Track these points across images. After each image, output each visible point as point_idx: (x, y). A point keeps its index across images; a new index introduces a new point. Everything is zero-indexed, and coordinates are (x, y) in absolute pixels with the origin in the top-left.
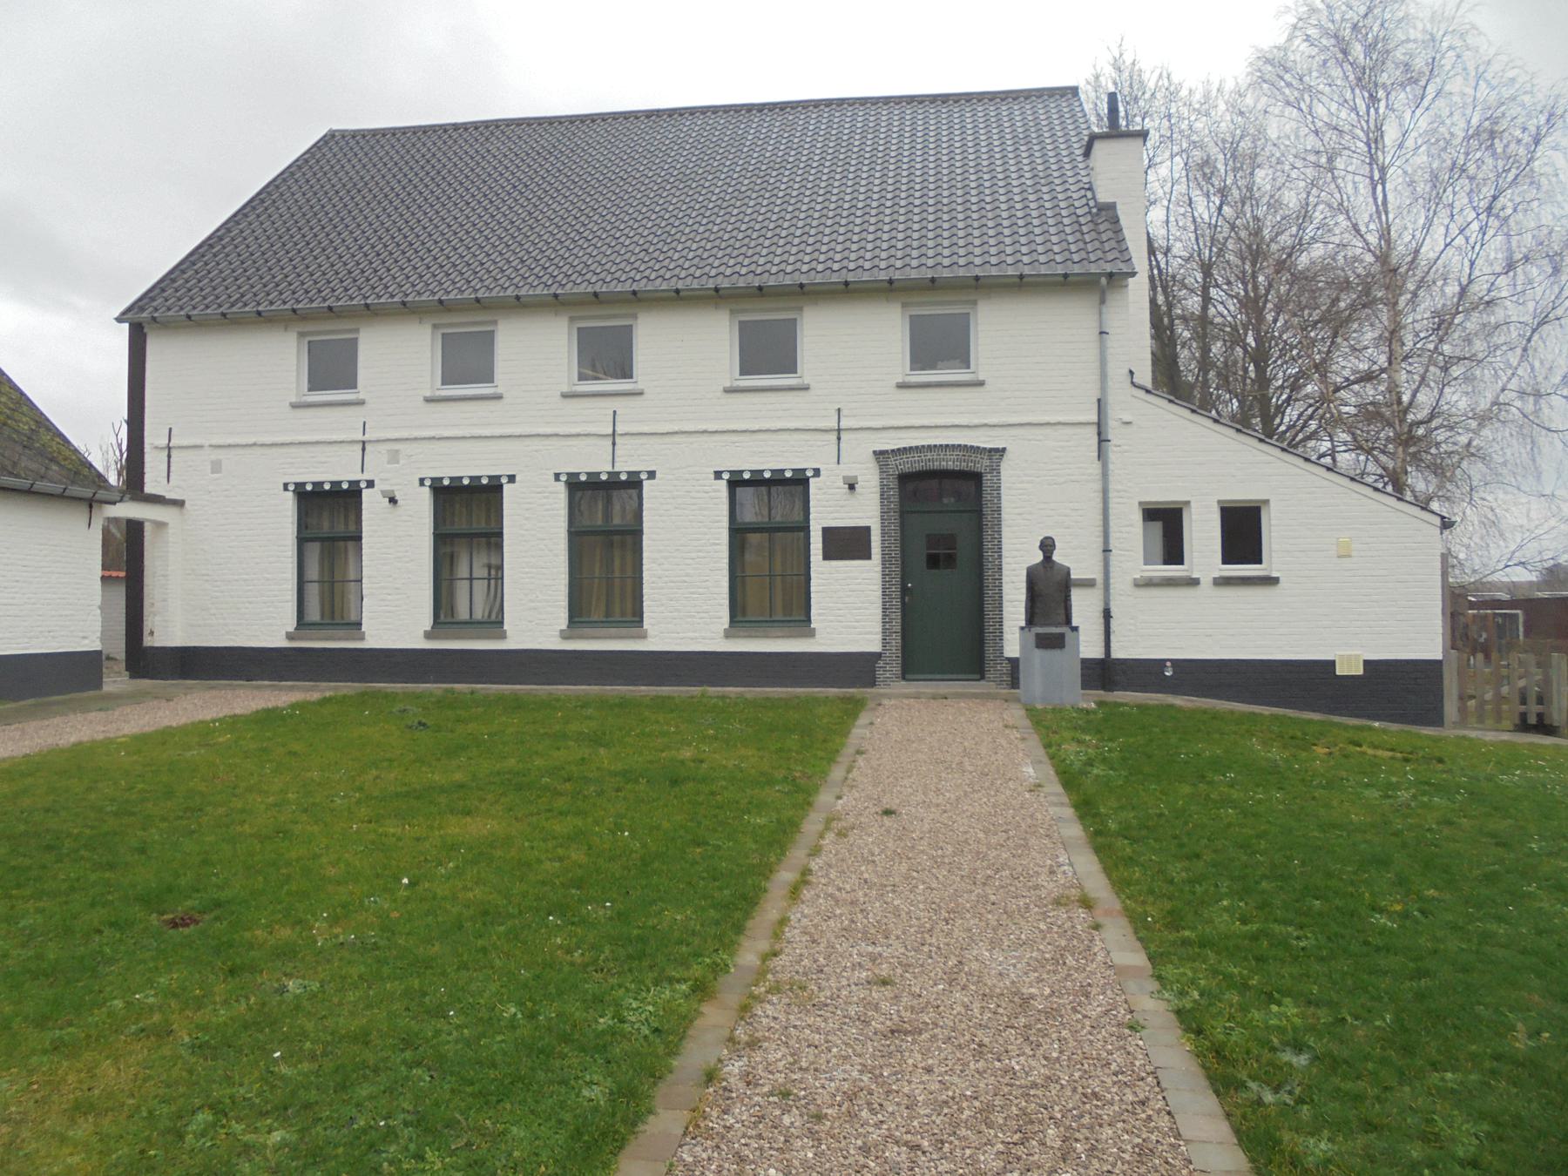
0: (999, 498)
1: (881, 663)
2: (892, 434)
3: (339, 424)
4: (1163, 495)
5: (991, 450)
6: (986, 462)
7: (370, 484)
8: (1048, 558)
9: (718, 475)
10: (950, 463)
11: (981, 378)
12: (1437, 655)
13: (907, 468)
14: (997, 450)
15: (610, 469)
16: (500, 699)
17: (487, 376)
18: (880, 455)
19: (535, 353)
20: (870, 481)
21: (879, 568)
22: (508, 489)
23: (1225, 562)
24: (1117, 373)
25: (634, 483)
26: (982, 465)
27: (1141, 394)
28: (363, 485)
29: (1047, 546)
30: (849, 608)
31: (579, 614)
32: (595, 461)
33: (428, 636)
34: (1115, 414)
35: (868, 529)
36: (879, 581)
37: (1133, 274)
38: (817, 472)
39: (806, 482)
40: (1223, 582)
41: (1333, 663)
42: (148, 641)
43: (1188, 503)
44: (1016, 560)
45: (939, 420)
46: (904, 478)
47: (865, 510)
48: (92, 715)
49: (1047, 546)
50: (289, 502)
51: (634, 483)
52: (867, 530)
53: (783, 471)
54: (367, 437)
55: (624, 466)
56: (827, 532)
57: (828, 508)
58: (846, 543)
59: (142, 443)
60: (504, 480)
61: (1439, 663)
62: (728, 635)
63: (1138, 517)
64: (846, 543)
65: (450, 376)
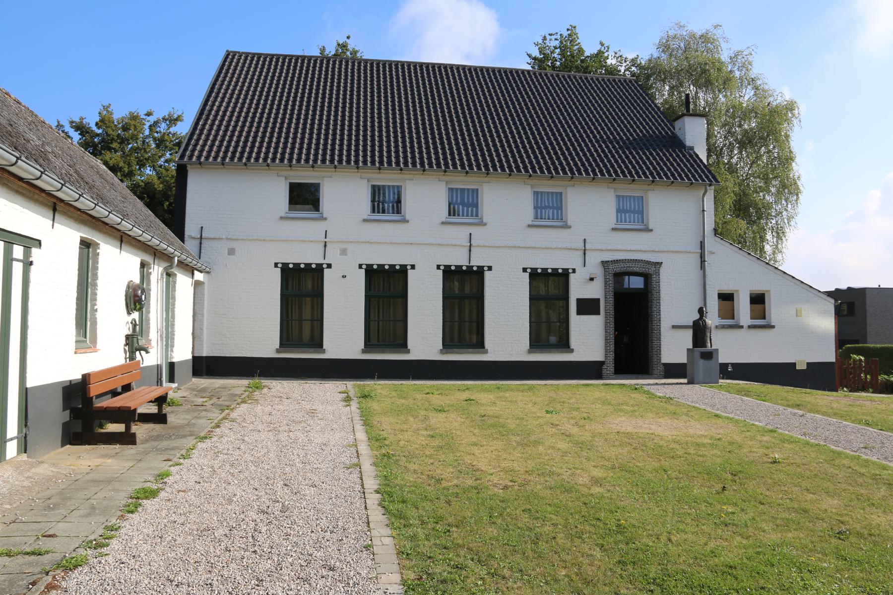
1: (605, 367)
2: (610, 253)
4: (727, 288)
6: (653, 269)
9: (525, 270)
12: (685, 362)
13: (618, 270)
14: (658, 263)
16: (630, 385)
18: (604, 263)
20: (599, 272)
22: (327, 272)
23: (751, 318)
25: (480, 272)
26: (652, 270)
28: (325, 266)
30: (589, 338)
31: (449, 343)
32: (458, 259)
33: (278, 351)
35: (598, 300)
38: (574, 271)
40: (750, 327)
41: (795, 364)
42: (829, 355)
43: (768, 291)
45: (631, 247)
47: (596, 291)
48: (840, 393)
50: (276, 275)
51: (480, 272)
52: (598, 300)
53: (300, 264)
55: (476, 262)
56: (579, 301)
57: (578, 289)
58: (588, 307)
61: (684, 365)
62: (442, 352)
64: (588, 307)
65: (452, 212)
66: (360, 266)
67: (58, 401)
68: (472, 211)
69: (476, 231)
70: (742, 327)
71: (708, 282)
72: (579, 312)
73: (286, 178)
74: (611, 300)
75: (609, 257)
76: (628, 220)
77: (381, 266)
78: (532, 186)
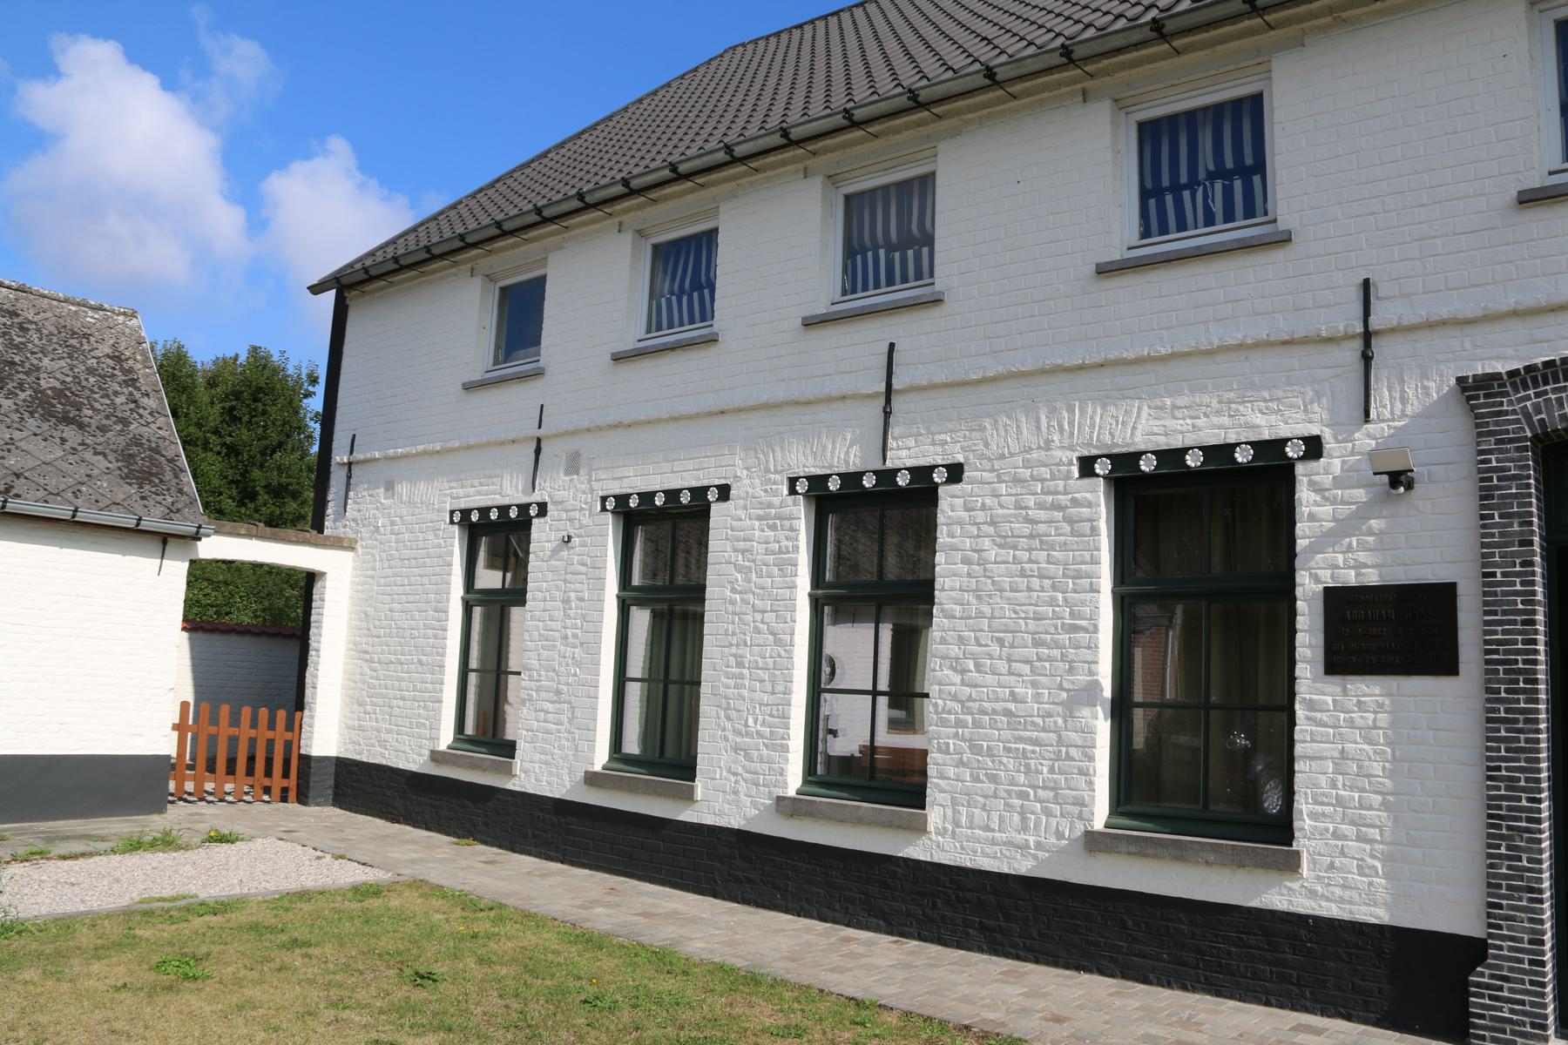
1: (1482, 975)
7: (955, 473)
15: (879, 466)
18: (1477, 391)
19: (1038, 199)
22: (950, 502)
32: (842, 453)
35: (1445, 594)
50: (1097, 504)
53: (1138, 455)
54: (358, 456)
55: (906, 454)
57: (1338, 544)
58: (1394, 631)
64: (1394, 631)
66: (1087, 466)
67: (311, 794)
68: (918, 259)
73: (640, 233)
75: (1501, 355)
76: (1218, 208)
77: (1171, 457)
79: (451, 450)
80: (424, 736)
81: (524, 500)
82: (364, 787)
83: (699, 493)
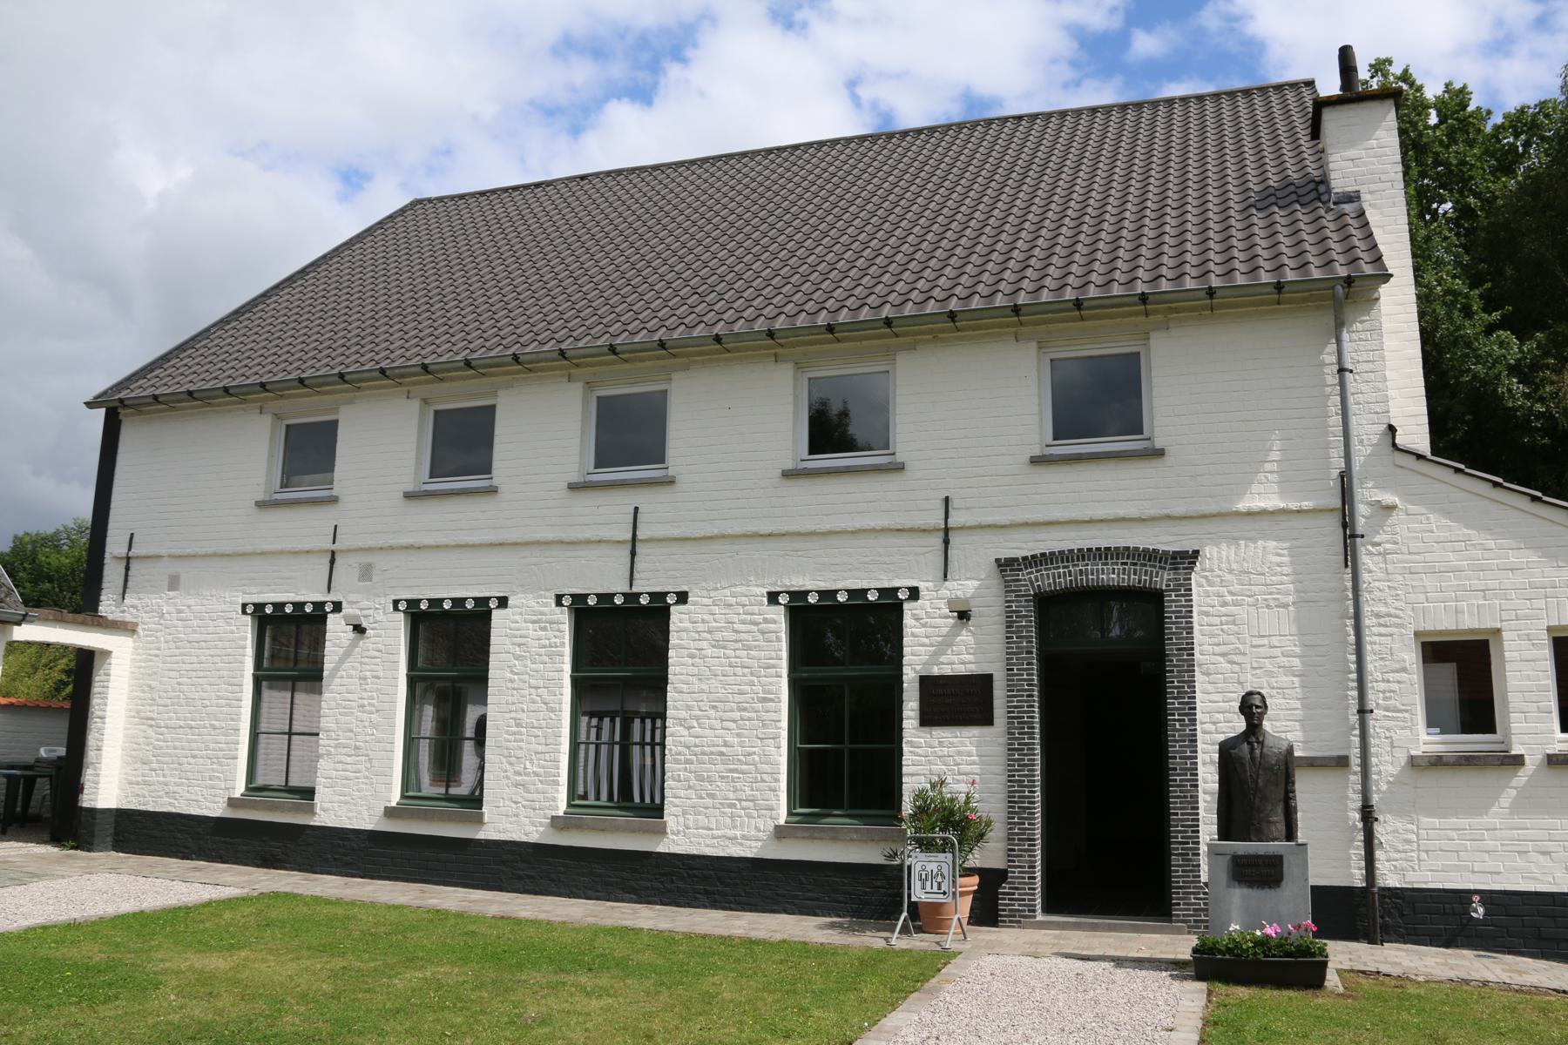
0: (1190, 630)
1: (1005, 888)
2: (1026, 534)
3: (306, 528)
5: (1175, 555)
7: (337, 607)
8: (1254, 727)
10: (1111, 575)
11: (1158, 445)
14: (1183, 555)
15: (626, 589)
17: (486, 469)
21: (1003, 740)
24: (1366, 431)
26: (1163, 579)
27: (1410, 461)
29: (1252, 707)
32: (605, 577)
34: (1367, 494)
35: (988, 679)
36: (1003, 759)
37: (1387, 277)
38: (914, 593)
39: (898, 609)
44: (1213, 721)
45: (1095, 509)
46: (1047, 603)
49: (1252, 707)
52: (988, 679)
55: (645, 585)
57: (930, 646)
58: (958, 701)
59: (103, 552)
60: (670, 600)
63: (1411, 657)
64: (958, 701)
65: (1064, 428)
69: (652, 504)
70: (1518, 761)
71: (291, 769)
72: (928, 719)
74: (1032, 674)
78: (798, 366)
79: (159, 557)
80: (212, 787)
81: (319, 598)
82: (144, 833)
83: (482, 602)
